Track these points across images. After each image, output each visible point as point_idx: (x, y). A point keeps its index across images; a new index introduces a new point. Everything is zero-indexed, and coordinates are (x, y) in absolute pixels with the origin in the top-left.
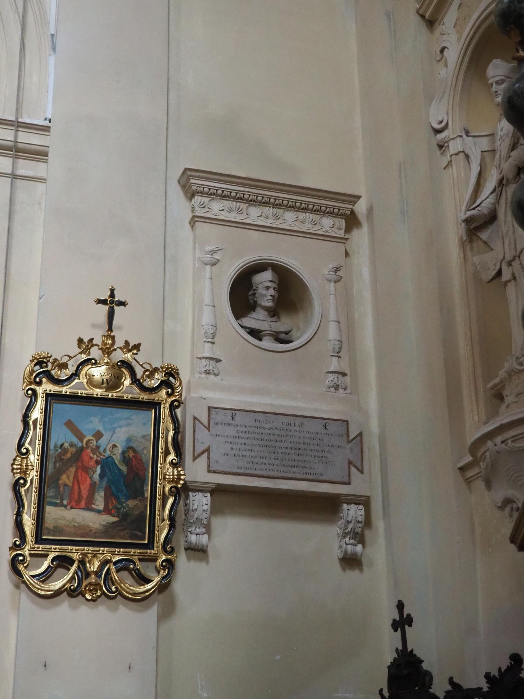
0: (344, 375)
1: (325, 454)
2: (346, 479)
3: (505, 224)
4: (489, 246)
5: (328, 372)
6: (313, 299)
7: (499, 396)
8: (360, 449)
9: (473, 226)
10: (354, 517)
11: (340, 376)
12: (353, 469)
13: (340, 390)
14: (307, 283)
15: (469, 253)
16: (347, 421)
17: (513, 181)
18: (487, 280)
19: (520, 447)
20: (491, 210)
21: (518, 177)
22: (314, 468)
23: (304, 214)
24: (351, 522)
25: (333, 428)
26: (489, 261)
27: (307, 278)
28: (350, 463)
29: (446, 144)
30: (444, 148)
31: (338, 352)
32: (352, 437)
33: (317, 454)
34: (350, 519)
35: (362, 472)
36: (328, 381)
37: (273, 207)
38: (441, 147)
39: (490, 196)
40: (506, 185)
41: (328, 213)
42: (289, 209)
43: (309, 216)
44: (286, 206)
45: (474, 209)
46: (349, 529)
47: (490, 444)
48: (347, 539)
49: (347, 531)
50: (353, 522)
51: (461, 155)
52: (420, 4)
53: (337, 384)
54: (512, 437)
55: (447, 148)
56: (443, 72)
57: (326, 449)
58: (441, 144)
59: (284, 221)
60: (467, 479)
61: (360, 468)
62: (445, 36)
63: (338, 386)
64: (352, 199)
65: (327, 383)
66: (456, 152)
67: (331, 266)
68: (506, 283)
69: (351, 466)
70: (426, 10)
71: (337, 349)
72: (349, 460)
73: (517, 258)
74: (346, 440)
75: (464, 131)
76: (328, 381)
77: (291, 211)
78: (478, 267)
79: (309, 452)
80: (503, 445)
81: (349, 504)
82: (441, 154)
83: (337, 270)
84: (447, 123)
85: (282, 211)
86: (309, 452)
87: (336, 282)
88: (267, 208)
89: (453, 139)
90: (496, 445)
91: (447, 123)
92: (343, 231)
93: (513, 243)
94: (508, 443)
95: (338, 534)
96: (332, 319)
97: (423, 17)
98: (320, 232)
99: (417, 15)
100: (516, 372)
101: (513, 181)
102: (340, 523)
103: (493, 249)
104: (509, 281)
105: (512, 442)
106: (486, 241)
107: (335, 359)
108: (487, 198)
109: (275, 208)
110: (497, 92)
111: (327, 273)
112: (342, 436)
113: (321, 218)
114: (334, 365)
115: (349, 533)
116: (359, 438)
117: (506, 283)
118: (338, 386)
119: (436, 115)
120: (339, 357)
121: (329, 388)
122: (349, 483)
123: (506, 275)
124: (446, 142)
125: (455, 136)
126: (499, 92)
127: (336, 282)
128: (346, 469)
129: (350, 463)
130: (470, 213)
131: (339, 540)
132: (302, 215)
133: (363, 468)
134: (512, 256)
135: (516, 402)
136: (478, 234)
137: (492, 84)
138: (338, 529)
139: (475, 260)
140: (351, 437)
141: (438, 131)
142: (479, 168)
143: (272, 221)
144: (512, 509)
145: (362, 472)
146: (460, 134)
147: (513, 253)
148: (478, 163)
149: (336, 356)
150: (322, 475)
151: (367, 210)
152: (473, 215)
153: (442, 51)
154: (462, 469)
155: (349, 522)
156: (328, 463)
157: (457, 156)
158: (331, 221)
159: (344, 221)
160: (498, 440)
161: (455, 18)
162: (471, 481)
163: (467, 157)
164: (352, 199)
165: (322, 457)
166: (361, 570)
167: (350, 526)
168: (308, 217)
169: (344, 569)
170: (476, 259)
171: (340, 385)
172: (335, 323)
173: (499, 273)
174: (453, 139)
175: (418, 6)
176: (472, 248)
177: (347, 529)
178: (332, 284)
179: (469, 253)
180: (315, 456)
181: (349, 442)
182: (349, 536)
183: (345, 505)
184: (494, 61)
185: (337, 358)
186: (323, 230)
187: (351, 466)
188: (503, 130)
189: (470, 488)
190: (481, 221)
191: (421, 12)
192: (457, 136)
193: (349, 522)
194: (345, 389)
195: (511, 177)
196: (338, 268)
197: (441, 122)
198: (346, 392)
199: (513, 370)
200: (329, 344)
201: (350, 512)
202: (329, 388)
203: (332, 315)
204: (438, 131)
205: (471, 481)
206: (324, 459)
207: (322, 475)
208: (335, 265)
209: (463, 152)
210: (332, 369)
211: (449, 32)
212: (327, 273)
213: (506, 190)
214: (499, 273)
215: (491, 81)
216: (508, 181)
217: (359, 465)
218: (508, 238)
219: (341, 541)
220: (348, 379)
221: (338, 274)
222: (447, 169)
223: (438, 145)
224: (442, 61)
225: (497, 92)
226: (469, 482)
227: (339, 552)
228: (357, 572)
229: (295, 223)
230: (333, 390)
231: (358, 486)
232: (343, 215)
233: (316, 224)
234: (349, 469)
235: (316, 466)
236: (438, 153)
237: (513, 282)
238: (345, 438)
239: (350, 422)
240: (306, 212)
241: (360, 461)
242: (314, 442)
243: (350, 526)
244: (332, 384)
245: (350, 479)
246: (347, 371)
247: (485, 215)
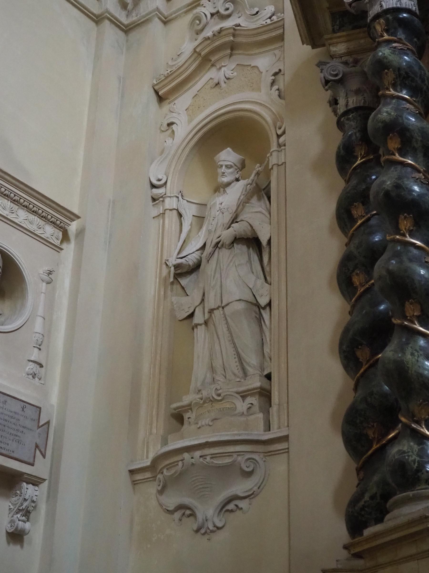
0: (41, 366)
1: (19, 434)
2: (31, 461)
3: (213, 279)
4: (185, 291)
5: (29, 361)
6: (28, 293)
7: (179, 418)
8: (46, 436)
9: (179, 271)
10: (31, 497)
11: (38, 366)
12: (38, 452)
13: (36, 379)
14: (25, 277)
15: (169, 293)
16: (40, 408)
17: (227, 247)
18: (180, 319)
19: (216, 464)
20: (194, 263)
21: (232, 245)
22: (8, 445)
23: (33, 217)
24: (27, 500)
25: (29, 411)
26: (186, 304)
27: (27, 273)
28: (37, 446)
29: (161, 199)
30: (157, 202)
31: (40, 345)
32: (41, 423)
33: (12, 432)
34: (27, 497)
35: (44, 456)
36: (28, 368)
37: (11, 201)
38: (154, 200)
39: (196, 252)
40: (219, 248)
41: (51, 222)
42: (23, 207)
43: (37, 220)
44: (21, 204)
45: (182, 258)
46: (24, 507)
47: (186, 456)
48: (19, 516)
49: (21, 508)
50: (29, 500)
51: (175, 212)
52: (158, 82)
53: (36, 373)
54: (211, 454)
55: (161, 202)
56: (169, 141)
57: (21, 429)
58: (155, 197)
59: (17, 217)
60: (134, 481)
61: (43, 452)
62: (174, 114)
63: (35, 374)
64: (72, 217)
65: (27, 369)
66: (171, 208)
67: (46, 269)
68: (197, 325)
69: (37, 449)
70: (161, 88)
71: (40, 343)
72: (36, 443)
73: (221, 309)
74: (37, 426)
75: (180, 194)
76: (28, 368)
77: (24, 209)
78: (175, 306)
79: (6, 428)
80: (201, 459)
81: (28, 483)
82: (153, 205)
83: (50, 273)
84: (166, 183)
85: (17, 207)
86: (6, 428)
87: (48, 283)
88: (6, 201)
89: (170, 197)
90: (192, 458)
91: (166, 183)
92: (59, 242)
93: (219, 295)
94: (206, 459)
95: (10, 509)
96: (39, 315)
97: (157, 92)
98: (42, 236)
99: (152, 89)
100: (211, 401)
101: (227, 247)
102: (14, 499)
103: (188, 295)
104: (201, 325)
105: (211, 458)
106: (184, 287)
107: (36, 350)
108: (193, 253)
109: (13, 203)
110: (224, 173)
111: (42, 273)
112: (34, 420)
113: (45, 224)
114: (35, 355)
115: (23, 510)
116: (46, 426)
117: (197, 325)
118: (35, 374)
119: (156, 173)
120: (40, 349)
121: (28, 375)
122: (33, 465)
123: (198, 318)
124: (162, 197)
125: (172, 195)
126: (226, 173)
127: (48, 283)
128: (33, 450)
129: (37, 446)
130: (180, 261)
131: (10, 515)
132: (32, 217)
133: (45, 453)
134: (217, 306)
135: (210, 426)
136: (179, 279)
137: (222, 166)
138: (10, 505)
139: (173, 300)
140: (41, 424)
141: (153, 186)
142: (190, 227)
143: (8, 213)
144: (184, 514)
145: (44, 456)
146: (177, 195)
147: (219, 304)
148: (190, 223)
149: (37, 347)
150: (13, 452)
151: (77, 230)
152: (182, 263)
153: (170, 124)
154: (132, 472)
155: (25, 500)
156: (20, 442)
157: (171, 212)
158: (52, 230)
159: (61, 233)
160: (197, 454)
161: (189, 104)
162: (137, 484)
163: (180, 215)
164: (72, 217)
165: (16, 436)
166: (22, 546)
167: (25, 504)
168: (36, 220)
169: (9, 543)
170: (174, 299)
171: (37, 375)
172: (42, 319)
173: (192, 315)
174: (170, 197)
175: (155, 83)
176: (172, 290)
177: (21, 506)
178: (44, 284)
179: (169, 293)
180: (11, 434)
181: (39, 427)
182: (21, 513)
183: (25, 484)
184: (228, 148)
185: (38, 350)
186: (45, 235)
187: (37, 449)
188: (223, 204)
189: (134, 489)
190: (185, 270)
191: (156, 88)
192: (174, 196)
193: (25, 500)
194: (40, 379)
195: (227, 243)
196: (51, 272)
197: (159, 180)
198: (40, 382)
199: (209, 398)
200: (34, 335)
201: (28, 491)
202: (28, 375)
203: (40, 312)
204: (153, 186)
205: (137, 484)
206: (17, 438)
207: (13, 452)
208: (50, 268)
209: (177, 210)
210: (33, 359)
211: (181, 112)
212: (42, 273)
213: (219, 252)
214: (192, 315)
215: (221, 163)
216: (222, 245)
217: (43, 450)
218: (215, 290)
219: (13, 516)
220: (43, 369)
221: (50, 276)
222: (155, 219)
223: (152, 198)
224: (166, 132)
225: (224, 173)
226: (135, 484)
227: (9, 526)
228: (18, 547)
229: (25, 221)
230: (31, 377)
231: (40, 469)
232: (62, 228)
233: (40, 228)
234: (35, 452)
235: (10, 442)
236: (151, 203)
237: (203, 326)
238: (36, 422)
239: (42, 409)
240: (35, 216)
241: (44, 446)
242: (12, 420)
243: (25, 504)
244: (32, 372)
245: (34, 461)
246: (44, 364)
247: (189, 265)
